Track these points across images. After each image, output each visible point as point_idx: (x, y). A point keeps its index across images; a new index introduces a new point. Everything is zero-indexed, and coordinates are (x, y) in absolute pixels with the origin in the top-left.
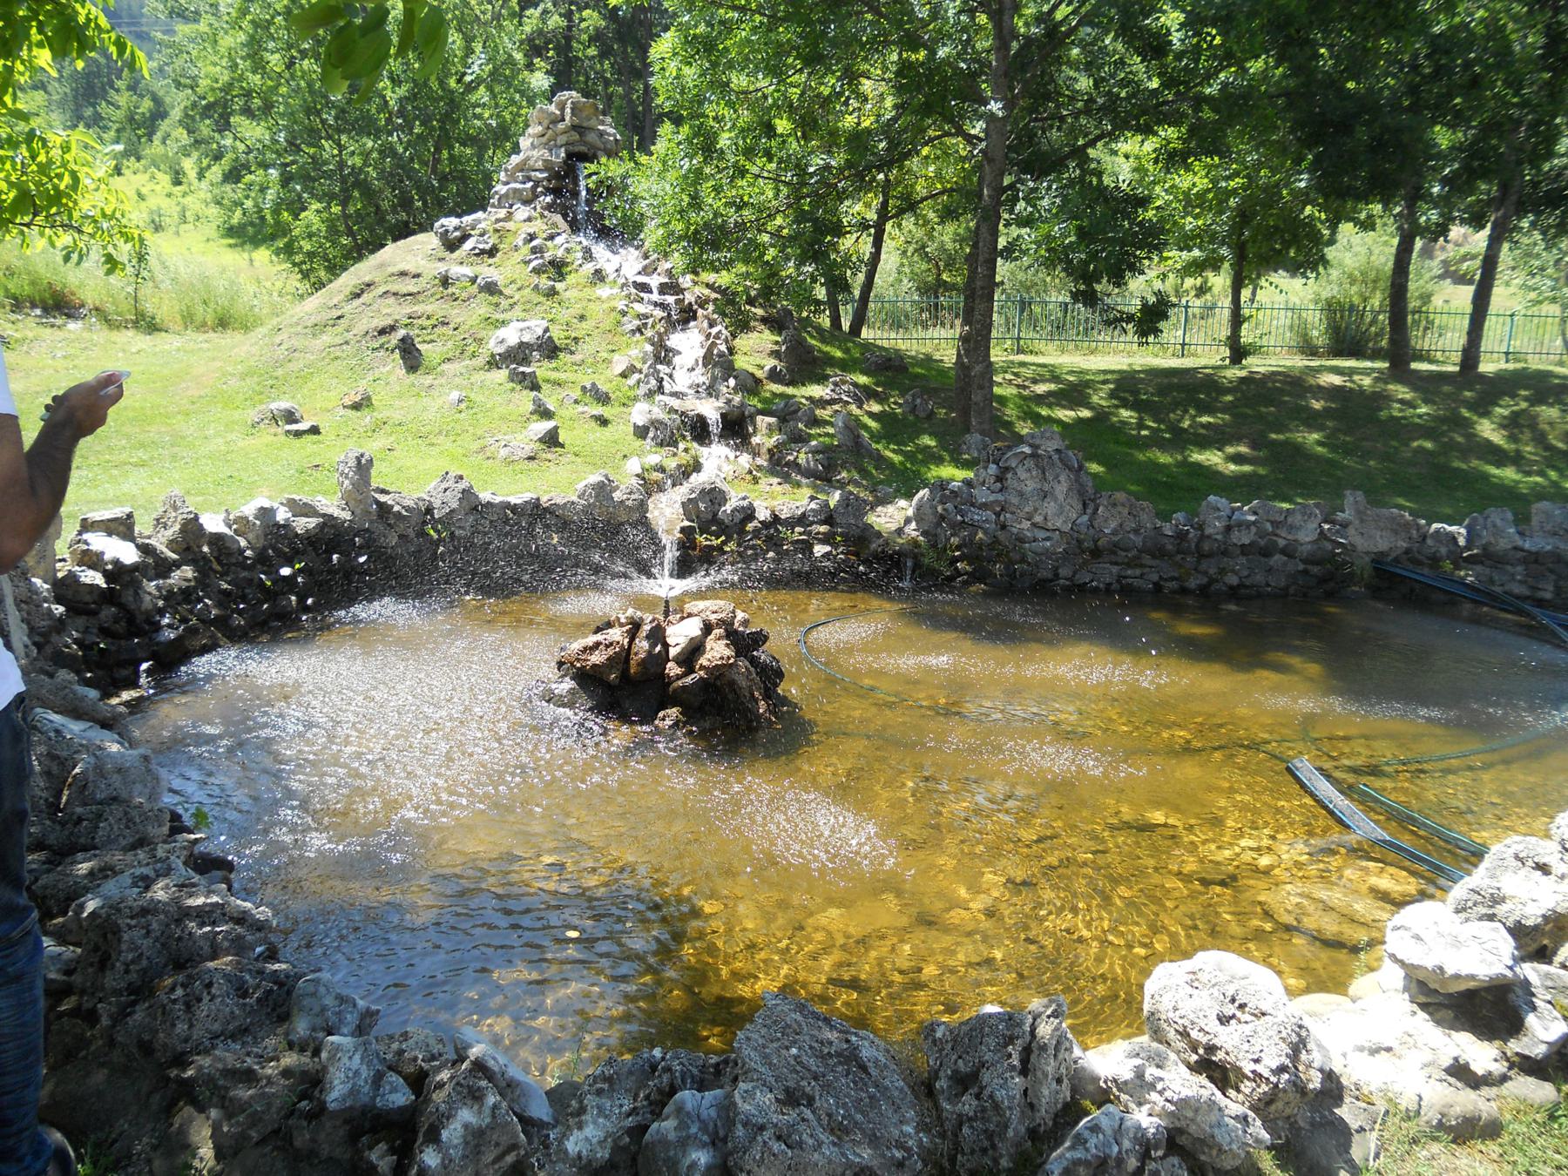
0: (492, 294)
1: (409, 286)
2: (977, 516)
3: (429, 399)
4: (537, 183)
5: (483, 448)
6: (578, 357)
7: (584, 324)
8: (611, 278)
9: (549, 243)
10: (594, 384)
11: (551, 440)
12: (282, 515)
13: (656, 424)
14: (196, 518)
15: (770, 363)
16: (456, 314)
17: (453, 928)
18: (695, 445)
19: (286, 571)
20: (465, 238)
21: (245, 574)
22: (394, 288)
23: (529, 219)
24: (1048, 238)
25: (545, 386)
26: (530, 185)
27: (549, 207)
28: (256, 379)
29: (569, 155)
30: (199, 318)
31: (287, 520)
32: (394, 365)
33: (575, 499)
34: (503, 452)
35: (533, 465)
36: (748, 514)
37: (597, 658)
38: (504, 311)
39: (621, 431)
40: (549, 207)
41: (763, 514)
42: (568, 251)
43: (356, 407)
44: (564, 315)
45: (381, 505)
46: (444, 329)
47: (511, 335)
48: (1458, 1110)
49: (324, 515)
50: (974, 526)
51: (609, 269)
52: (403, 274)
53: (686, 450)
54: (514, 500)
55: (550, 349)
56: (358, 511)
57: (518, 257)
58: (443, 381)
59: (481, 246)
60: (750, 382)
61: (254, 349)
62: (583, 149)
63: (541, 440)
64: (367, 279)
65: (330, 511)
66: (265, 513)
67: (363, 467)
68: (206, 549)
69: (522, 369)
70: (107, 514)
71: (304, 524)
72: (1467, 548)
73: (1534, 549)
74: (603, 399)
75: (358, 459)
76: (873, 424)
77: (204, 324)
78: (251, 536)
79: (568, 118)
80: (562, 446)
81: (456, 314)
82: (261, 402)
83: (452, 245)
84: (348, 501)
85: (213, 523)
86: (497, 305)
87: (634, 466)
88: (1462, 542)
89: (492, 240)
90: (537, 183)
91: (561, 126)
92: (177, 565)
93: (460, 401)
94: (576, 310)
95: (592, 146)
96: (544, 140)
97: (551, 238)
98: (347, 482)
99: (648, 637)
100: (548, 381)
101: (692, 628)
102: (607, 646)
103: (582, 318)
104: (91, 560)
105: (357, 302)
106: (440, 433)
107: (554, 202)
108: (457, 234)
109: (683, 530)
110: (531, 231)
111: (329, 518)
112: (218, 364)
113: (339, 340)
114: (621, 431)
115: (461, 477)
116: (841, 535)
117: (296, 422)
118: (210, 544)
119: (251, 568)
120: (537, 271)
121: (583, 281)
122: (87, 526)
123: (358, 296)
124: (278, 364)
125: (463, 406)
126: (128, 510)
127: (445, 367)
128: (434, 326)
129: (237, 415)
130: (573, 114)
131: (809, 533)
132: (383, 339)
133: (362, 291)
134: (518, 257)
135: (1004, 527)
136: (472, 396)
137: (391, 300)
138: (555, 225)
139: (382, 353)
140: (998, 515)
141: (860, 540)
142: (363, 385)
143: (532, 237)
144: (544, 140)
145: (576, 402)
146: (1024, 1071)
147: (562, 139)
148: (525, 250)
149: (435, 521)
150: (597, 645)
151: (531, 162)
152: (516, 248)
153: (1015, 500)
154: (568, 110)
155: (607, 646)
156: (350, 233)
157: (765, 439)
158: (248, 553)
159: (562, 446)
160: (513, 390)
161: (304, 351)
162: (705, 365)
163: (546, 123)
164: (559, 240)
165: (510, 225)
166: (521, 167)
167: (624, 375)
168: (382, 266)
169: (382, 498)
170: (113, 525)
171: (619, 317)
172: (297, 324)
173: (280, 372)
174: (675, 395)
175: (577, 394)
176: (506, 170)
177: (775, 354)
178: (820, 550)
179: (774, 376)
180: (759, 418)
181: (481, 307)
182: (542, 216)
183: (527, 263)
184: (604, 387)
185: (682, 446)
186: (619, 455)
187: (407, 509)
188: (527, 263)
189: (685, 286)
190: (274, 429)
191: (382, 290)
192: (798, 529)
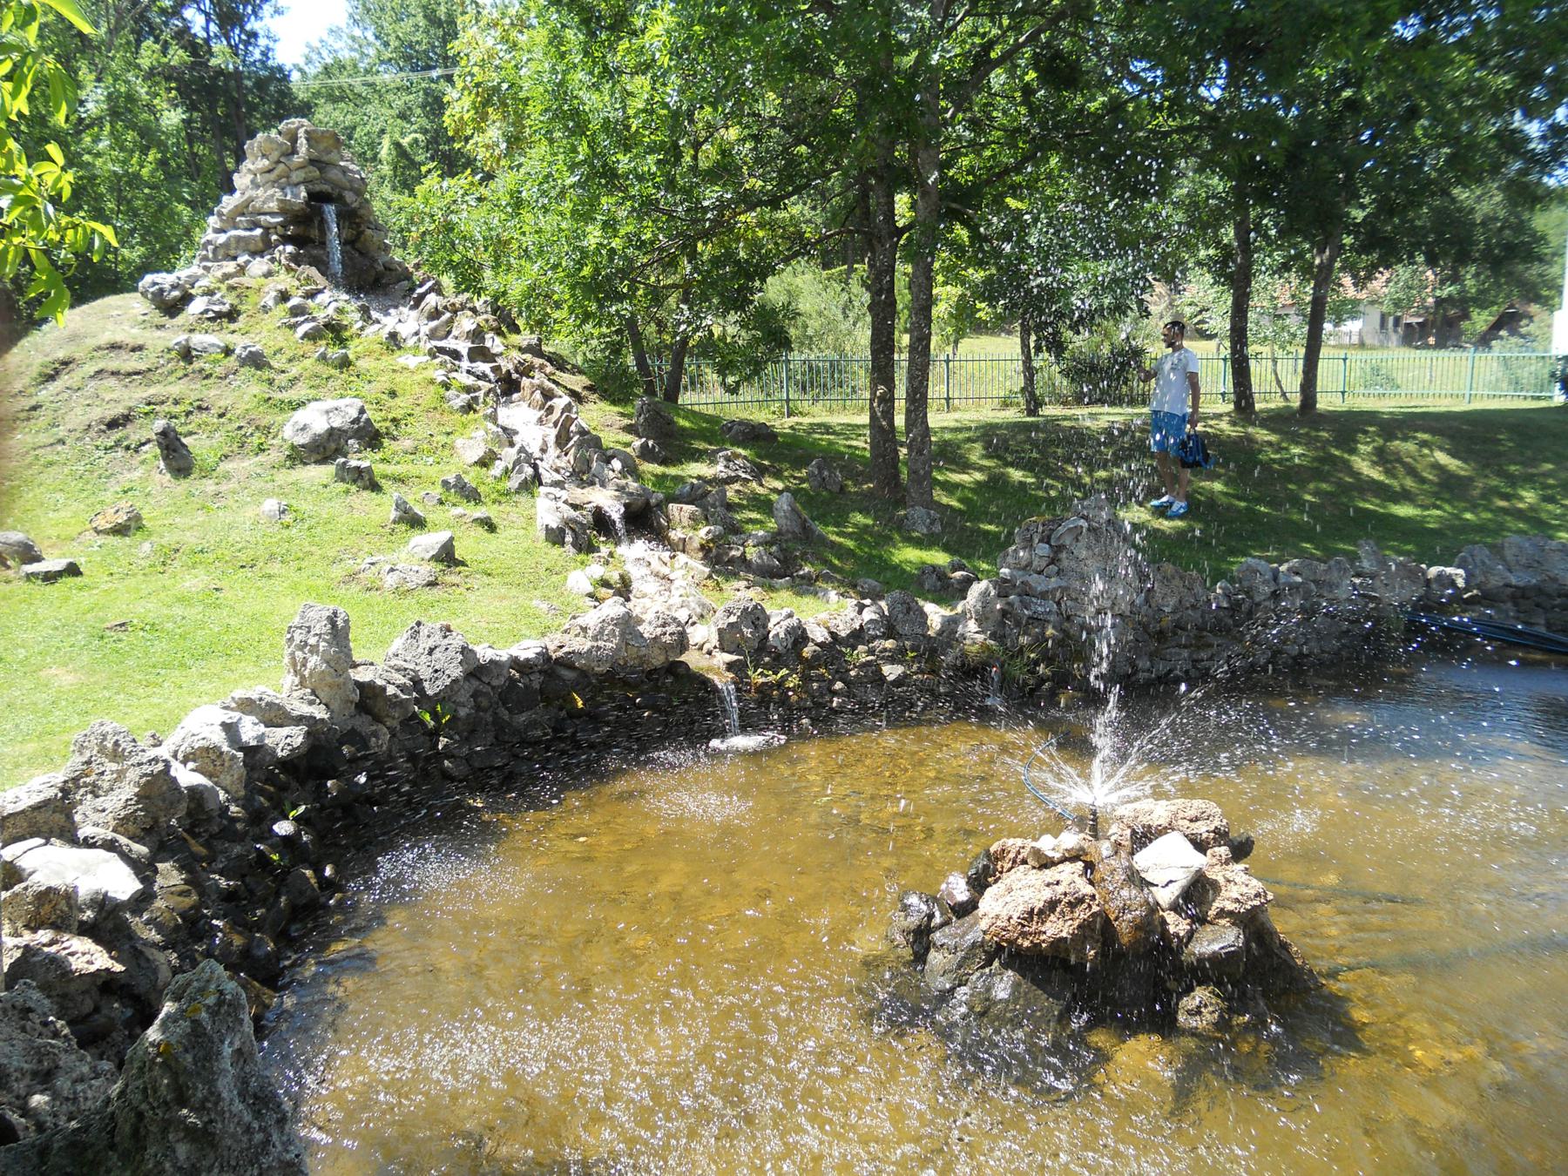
0: (259, 367)
1: (131, 363)
4: (267, 230)
6: (408, 444)
8: (411, 342)
10: (459, 477)
16: (216, 394)
20: (187, 298)
22: (113, 365)
23: (268, 274)
24: (1063, 271)
26: (258, 231)
29: (312, 196)
34: (391, 580)
36: (799, 636)
37: (1057, 928)
38: (280, 389)
40: (295, 259)
41: (819, 635)
43: (120, 530)
52: (114, 347)
55: (371, 437)
56: (335, 706)
58: (233, 485)
59: (216, 308)
62: (326, 188)
64: (61, 354)
67: (338, 633)
72: (1466, 590)
73: (1521, 584)
75: (332, 620)
80: (463, 563)
81: (216, 394)
88: (1461, 583)
89: (230, 300)
90: (267, 230)
94: (383, 383)
95: (335, 185)
96: (273, 176)
100: (385, 477)
102: (1072, 905)
103: (393, 394)
105: (53, 387)
106: (272, 557)
108: (176, 293)
117: (38, 559)
123: (51, 378)
125: (288, 518)
127: (226, 466)
128: (188, 414)
132: (117, 434)
133: (57, 372)
139: (120, 453)
141: (930, 650)
143: (284, 297)
144: (273, 176)
147: (297, 176)
154: (302, 141)
155: (1072, 905)
159: (463, 563)
160: (347, 492)
163: (275, 155)
164: (323, 298)
166: (241, 210)
170: (40, 817)
171: (442, 391)
175: (437, 491)
176: (220, 214)
178: (892, 671)
183: (293, 327)
189: (495, 350)
191: (91, 368)
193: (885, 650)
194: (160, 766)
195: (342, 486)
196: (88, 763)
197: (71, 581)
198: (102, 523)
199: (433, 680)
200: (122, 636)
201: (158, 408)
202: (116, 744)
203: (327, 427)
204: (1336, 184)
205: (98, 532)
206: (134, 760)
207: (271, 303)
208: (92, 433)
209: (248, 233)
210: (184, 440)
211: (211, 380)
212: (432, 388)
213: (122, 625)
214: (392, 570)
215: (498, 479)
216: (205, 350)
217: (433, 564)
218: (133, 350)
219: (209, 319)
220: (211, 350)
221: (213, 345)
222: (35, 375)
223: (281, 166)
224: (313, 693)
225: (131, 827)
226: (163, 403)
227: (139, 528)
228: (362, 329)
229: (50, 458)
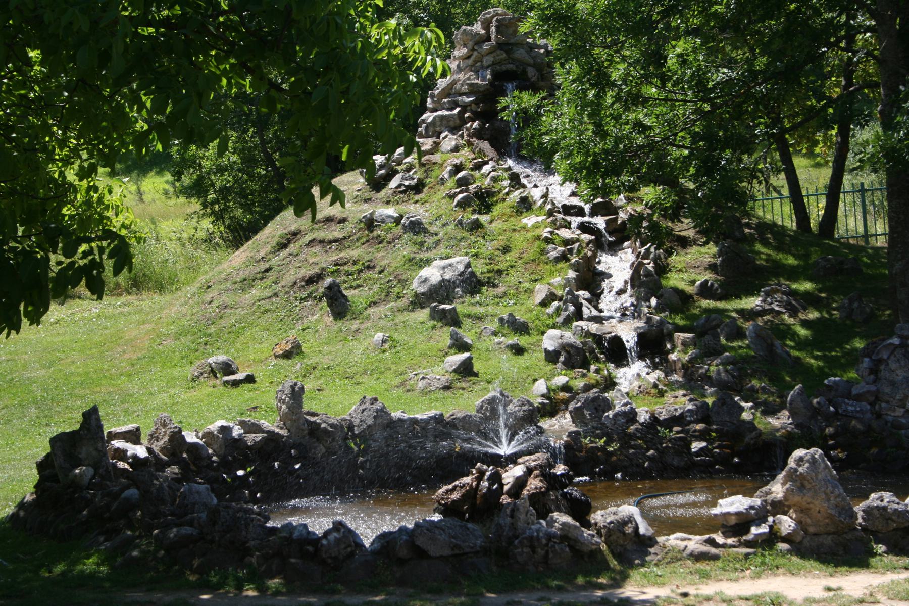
0: (417, 233)
1: (336, 232)
2: (851, 407)
3: (355, 343)
5: (403, 383)
6: (500, 290)
7: (508, 257)
9: (477, 174)
10: (511, 315)
11: (466, 370)
12: (237, 431)
13: (566, 348)
14: (180, 431)
15: (708, 276)
17: (304, 330)
18: (611, 366)
19: (240, 473)
21: (212, 473)
25: (467, 322)
27: (479, 134)
28: (189, 337)
29: (496, 76)
31: (240, 435)
32: (321, 315)
33: (474, 413)
34: (421, 384)
35: (448, 394)
37: (455, 496)
39: (534, 358)
41: (643, 416)
42: (495, 180)
43: (287, 355)
44: (488, 248)
45: (311, 423)
46: (370, 274)
47: (433, 274)
48: (699, 550)
49: (268, 432)
50: (848, 416)
51: (536, 194)
53: (597, 371)
54: (419, 416)
57: (444, 191)
59: (407, 183)
60: (675, 299)
61: (184, 310)
63: (455, 371)
65: (272, 428)
66: (225, 430)
67: (297, 394)
68: (185, 455)
69: (442, 306)
70: (124, 429)
71: (252, 438)
74: (521, 328)
76: (803, 332)
78: (215, 447)
79: (493, 37)
80: (476, 375)
82: (197, 359)
83: (377, 184)
84: (285, 420)
85: (190, 437)
86: (422, 244)
87: (541, 387)
89: (417, 174)
91: (486, 46)
92: (167, 464)
93: (384, 342)
96: (470, 61)
97: (478, 167)
98: (284, 406)
99: (488, 479)
100: (469, 316)
101: (517, 471)
103: (506, 250)
105: (284, 253)
106: (365, 372)
107: (482, 127)
109: (570, 434)
110: (457, 161)
111: (271, 433)
112: (150, 327)
113: (268, 293)
114: (534, 358)
115: (376, 400)
116: (716, 431)
117: (233, 373)
118: (188, 452)
119: (216, 469)
120: (463, 204)
121: (509, 210)
123: (283, 246)
124: (210, 321)
125: (387, 346)
126: (136, 425)
127: (371, 310)
128: (360, 271)
129: (176, 372)
130: (498, 31)
131: (687, 432)
132: (311, 288)
133: (289, 241)
134: (444, 191)
135: (879, 416)
136: (396, 336)
137: (317, 249)
138: (481, 153)
140: (872, 404)
142: (292, 334)
143: (458, 168)
144: (470, 61)
145: (495, 334)
146: (512, 516)
147: (488, 60)
148: (451, 183)
149: (354, 437)
150: (455, 488)
151: (458, 86)
152: (443, 182)
153: (887, 390)
154: (493, 29)
155: (461, 487)
156: (269, 161)
157: (681, 355)
158: (214, 458)
159: (476, 375)
160: (434, 327)
161: (235, 306)
162: (633, 287)
163: (470, 44)
164: (486, 169)
165: (437, 157)
166: (448, 92)
167: (544, 304)
169: (312, 419)
170: (128, 436)
172: (226, 280)
173: (212, 329)
174: (598, 320)
175: (494, 325)
176: (432, 97)
177: (712, 267)
179: (706, 291)
180: (676, 334)
181: (405, 249)
182: (469, 144)
183: (452, 197)
185: (593, 367)
186: (530, 379)
187: (332, 425)
188: (452, 197)
190: (212, 382)
191: (308, 238)
192: (676, 429)
193: (695, 431)
194: (177, 430)
195: (433, 322)
196: (157, 429)
197: (251, 386)
198: (279, 351)
199: (359, 426)
200: (253, 413)
201: (342, 268)
202: (164, 421)
203: (440, 278)
204: (720, 141)
205: (276, 356)
206: (169, 427)
207: (446, 176)
208: (296, 289)
209: (450, 112)
210: (345, 293)
211: (385, 244)
212: (537, 243)
213: (255, 408)
214: (423, 378)
215: (550, 316)
216: (383, 221)
217: (453, 375)
218: (340, 222)
219: (401, 192)
220: (388, 220)
221: (389, 216)
222: (274, 245)
223: (475, 53)
224: (284, 424)
225: (165, 451)
226: (345, 264)
227: (298, 354)
228: (508, 194)
229: (267, 307)
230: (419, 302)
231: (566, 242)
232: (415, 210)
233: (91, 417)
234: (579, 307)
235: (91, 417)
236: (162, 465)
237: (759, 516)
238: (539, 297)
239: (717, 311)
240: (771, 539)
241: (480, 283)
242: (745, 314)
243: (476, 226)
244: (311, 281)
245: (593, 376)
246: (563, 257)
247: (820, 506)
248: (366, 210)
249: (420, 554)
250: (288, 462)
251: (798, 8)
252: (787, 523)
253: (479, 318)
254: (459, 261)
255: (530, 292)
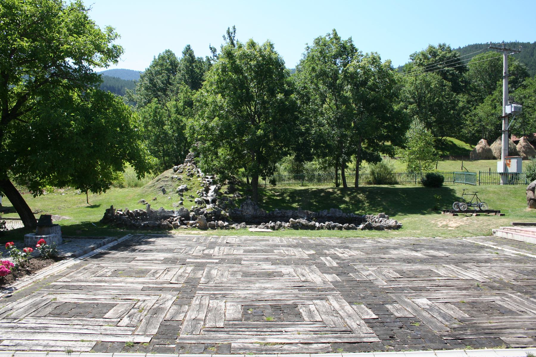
12: (139, 211)
20: (178, 169)
30: (131, 185)
39: (194, 202)
41: (205, 212)
43: (154, 200)
47: (180, 187)
52: (166, 177)
57: (186, 173)
60: (220, 194)
66: (137, 211)
71: (141, 212)
74: (193, 197)
77: (132, 186)
83: (175, 171)
85: (130, 211)
87: (192, 207)
97: (192, 169)
101: (176, 218)
103: (194, 184)
104: (118, 213)
114: (194, 202)
120: (188, 176)
122: (117, 210)
123: (158, 181)
124: (143, 193)
129: (136, 202)
135: (242, 214)
137: (163, 182)
138: (193, 167)
143: (189, 169)
152: (186, 171)
161: (148, 191)
164: (194, 170)
165: (186, 167)
166: (190, 156)
167: (198, 194)
168: (163, 175)
175: (188, 197)
179: (226, 193)
181: (177, 183)
184: (193, 196)
230: (177, 192)
231: (204, 183)
232: (181, 176)
233: (112, 207)
234: (203, 194)
235: (112, 207)
236: (125, 215)
237: (195, 224)
238: (197, 192)
239: (226, 196)
240: (196, 226)
241: (188, 189)
242: (230, 197)
243: (189, 180)
244: (161, 187)
245: (202, 206)
246: (203, 186)
247: (202, 223)
248: (172, 176)
249: (148, 226)
250: (146, 216)
251: (354, 123)
252: (198, 225)
253: (186, 195)
254: (185, 186)
255: (196, 191)
